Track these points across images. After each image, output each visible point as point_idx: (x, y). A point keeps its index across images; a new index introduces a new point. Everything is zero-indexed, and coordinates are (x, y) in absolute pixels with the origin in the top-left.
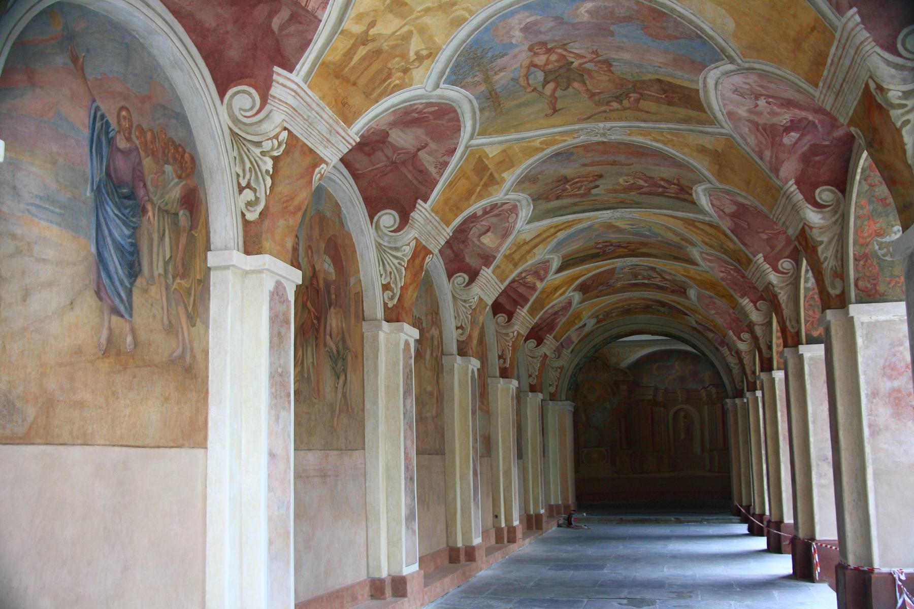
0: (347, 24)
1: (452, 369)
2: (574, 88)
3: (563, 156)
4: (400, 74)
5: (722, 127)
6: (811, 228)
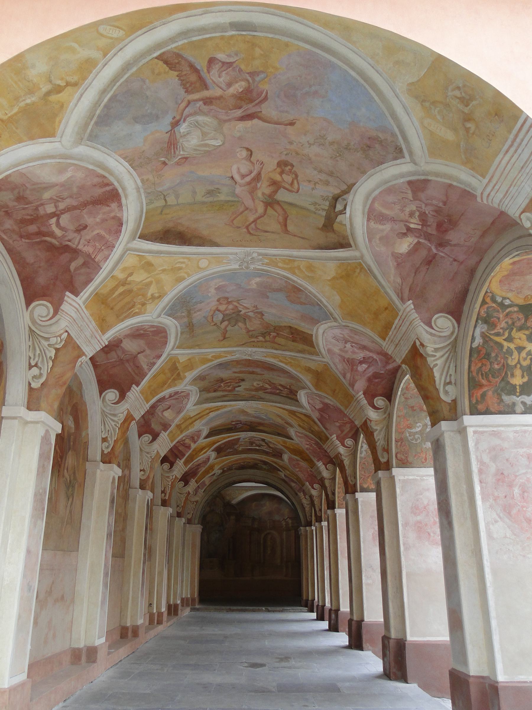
0: (116, 273)
1: (135, 498)
2: (239, 326)
3: (222, 366)
4: (139, 306)
5: (323, 358)
6: (371, 421)
